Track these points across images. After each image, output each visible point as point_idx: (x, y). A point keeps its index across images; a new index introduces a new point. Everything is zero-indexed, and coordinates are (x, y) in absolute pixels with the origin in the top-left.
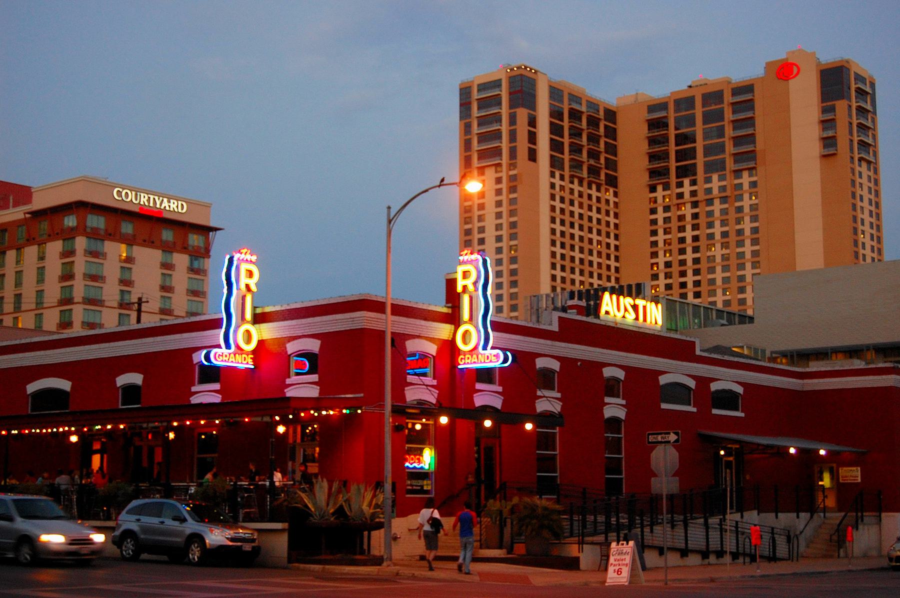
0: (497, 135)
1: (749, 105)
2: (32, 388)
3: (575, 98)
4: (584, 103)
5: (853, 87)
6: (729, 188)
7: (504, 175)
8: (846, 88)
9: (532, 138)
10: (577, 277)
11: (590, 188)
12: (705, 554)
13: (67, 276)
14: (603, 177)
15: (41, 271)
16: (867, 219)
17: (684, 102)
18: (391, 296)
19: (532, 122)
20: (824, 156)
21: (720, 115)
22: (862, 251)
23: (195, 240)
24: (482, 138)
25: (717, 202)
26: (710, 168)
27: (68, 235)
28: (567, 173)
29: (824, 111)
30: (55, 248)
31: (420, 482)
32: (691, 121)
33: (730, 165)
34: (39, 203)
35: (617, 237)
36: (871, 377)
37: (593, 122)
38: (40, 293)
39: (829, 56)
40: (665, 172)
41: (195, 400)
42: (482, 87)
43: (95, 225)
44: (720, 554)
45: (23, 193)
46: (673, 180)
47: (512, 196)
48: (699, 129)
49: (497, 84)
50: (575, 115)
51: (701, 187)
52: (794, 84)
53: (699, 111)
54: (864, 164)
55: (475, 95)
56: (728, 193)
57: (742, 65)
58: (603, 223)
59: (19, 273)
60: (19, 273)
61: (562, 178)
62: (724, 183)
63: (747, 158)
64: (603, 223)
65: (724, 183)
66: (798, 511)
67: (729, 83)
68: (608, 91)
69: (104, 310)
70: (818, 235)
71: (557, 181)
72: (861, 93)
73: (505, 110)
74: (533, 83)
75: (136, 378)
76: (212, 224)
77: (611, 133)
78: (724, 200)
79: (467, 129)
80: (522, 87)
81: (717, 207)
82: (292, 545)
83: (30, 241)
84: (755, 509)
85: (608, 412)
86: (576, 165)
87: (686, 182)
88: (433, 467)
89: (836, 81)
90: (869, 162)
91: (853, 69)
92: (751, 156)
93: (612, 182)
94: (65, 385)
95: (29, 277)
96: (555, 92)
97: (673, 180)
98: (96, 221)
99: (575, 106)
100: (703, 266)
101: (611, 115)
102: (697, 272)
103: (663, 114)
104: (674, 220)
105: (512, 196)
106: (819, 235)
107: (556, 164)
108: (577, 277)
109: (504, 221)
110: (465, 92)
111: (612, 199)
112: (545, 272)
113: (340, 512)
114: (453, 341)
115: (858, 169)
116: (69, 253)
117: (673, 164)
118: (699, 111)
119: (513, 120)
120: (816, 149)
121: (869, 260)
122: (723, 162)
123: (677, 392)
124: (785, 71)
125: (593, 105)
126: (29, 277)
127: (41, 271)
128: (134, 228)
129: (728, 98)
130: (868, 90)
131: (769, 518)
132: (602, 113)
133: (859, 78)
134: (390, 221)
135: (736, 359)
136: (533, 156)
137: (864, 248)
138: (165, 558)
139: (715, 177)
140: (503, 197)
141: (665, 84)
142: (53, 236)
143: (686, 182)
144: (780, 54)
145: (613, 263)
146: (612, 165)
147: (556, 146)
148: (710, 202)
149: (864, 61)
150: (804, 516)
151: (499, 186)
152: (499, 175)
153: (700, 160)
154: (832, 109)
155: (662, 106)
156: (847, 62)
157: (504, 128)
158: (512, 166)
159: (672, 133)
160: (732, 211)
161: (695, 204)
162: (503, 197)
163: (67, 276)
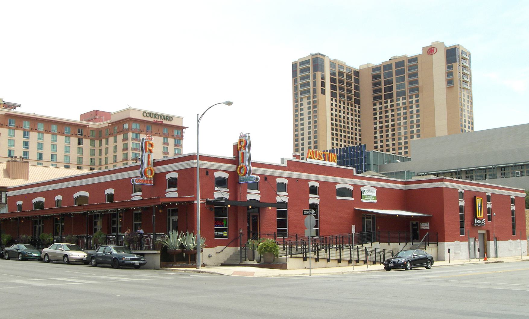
0: (308, 84)
1: (416, 67)
2: (75, 196)
3: (341, 66)
4: (345, 68)
5: (461, 56)
6: (407, 103)
7: (311, 100)
8: (457, 57)
9: (323, 84)
10: (343, 143)
11: (348, 105)
12: (350, 262)
13: (125, 148)
14: (353, 100)
15: (115, 147)
16: (467, 114)
17: (387, 66)
18: (200, 152)
19: (323, 78)
20: (448, 88)
21: (403, 72)
22: (464, 129)
23: (176, 132)
24: (302, 86)
25: (402, 109)
26: (399, 94)
27: (125, 132)
28: (338, 99)
29: (448, 68)
30: (120, 137)
31: (222, 233)
32: (390, 75)
33: (407, 93)
34: (114, 119)
35: (359, 126)
36: (434, 183)
37: (349, 76)
38: (115, 157)
39: (449, 44)
40: (380, 97)
41: (133, 199)
42: (302, 63)
43: (135, 128)
44: (357, 261)
45: (107, 115)
46: (383, 100)
47: (314, 109)
48: (394, 78)
49: (307, 62)
50: (341, 74)
51: (395, 103)
52: (434, 56)
53: (394, 70)
54: (465, 91)
55: (299, 67)
56: (406, 105)
57: (412, 49)
58: (354, 120)
59: (107, 149)
60: (107, 149)
61: (336, 101)
62: (405, 101)
63: (415, 90)
64: (354, 120)
65: (405, 101)
66: (399, 242)
67: (407, 57)
68: (355, 62)
69: (44, 163)
70: (445, 122)
71: (334, 103)
72: (464, 59)
73: (311, 73)
74: (323, 61)
75: (111, 191)
76: (184, 126)
77: (357, 81)
78: (405, 108)
79: (295, 81)
80: (317, 62)
81: (402, 111)
82: (162, 260)
83: (111, 135)
84: (377, 241)
85: (311, 201)
86: (341, 96)
87: (389, 101)
88: (2, 235)
89: (452, 54)
90: (467, 90)
91: (461, 49)
92: (417, 89)
93: (357, 102)
94: (87, 194)
95: (111, 150)
96: (333, 64)
97: (383, 100)
98: (135, 126)
99: (341, 70)
100: (396, 137)
101: (357, 73)
102: (394, 140)
103: (378, 72)
104: (408, 117)
105: (314, 109)
106: (437, 123)
107: (333, 95)
108: (343, 143)
109: (311, 120)
110: (295, 65)
111: (357, 109)
112: (329, 141)
113: (182, 246)
114: (236, 172)
115: (463, 92)
116: (126, 139)
117: (383, 93)
118: (394, 70)
119: (315, 77)
120: (444, 84)
121: (467, 132)
122: (404, 92)
123: (343, 192)
124: (431, 51)
125: (349, 68)
126: (111, 150)
127: (115, 147)
128: (44, 127)
129: (406, 64)
130: (467, 57)
131: (385, 245)
132: (353, 73)
133: (463, 52)
134: (198, 121)
135: (373, 177)
136: (323, 92)
137: (465, 127)
138: (110, 265)
139: (401, 98)
140: (311, 110)
141: (378, 58)
142: (119, 133)
143: (389, 101)
144: (428, 44)
145: (358, 137)
146: (357, 95)
147: (333, 87)
148: (399, 109)
149: (465, 43)
150: (403, 244)
151: (309, 106)
152: (309, 101)
153: (395, 92)
154: (451, 67)
155: (377, 68)
156: (458, 45)
157: (311, 80)
158: (315, 97)
159: (383, 80)
160: (408, 113)
161: (393, 111)
162: (311, 110)
163: (125, 148)
